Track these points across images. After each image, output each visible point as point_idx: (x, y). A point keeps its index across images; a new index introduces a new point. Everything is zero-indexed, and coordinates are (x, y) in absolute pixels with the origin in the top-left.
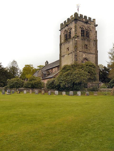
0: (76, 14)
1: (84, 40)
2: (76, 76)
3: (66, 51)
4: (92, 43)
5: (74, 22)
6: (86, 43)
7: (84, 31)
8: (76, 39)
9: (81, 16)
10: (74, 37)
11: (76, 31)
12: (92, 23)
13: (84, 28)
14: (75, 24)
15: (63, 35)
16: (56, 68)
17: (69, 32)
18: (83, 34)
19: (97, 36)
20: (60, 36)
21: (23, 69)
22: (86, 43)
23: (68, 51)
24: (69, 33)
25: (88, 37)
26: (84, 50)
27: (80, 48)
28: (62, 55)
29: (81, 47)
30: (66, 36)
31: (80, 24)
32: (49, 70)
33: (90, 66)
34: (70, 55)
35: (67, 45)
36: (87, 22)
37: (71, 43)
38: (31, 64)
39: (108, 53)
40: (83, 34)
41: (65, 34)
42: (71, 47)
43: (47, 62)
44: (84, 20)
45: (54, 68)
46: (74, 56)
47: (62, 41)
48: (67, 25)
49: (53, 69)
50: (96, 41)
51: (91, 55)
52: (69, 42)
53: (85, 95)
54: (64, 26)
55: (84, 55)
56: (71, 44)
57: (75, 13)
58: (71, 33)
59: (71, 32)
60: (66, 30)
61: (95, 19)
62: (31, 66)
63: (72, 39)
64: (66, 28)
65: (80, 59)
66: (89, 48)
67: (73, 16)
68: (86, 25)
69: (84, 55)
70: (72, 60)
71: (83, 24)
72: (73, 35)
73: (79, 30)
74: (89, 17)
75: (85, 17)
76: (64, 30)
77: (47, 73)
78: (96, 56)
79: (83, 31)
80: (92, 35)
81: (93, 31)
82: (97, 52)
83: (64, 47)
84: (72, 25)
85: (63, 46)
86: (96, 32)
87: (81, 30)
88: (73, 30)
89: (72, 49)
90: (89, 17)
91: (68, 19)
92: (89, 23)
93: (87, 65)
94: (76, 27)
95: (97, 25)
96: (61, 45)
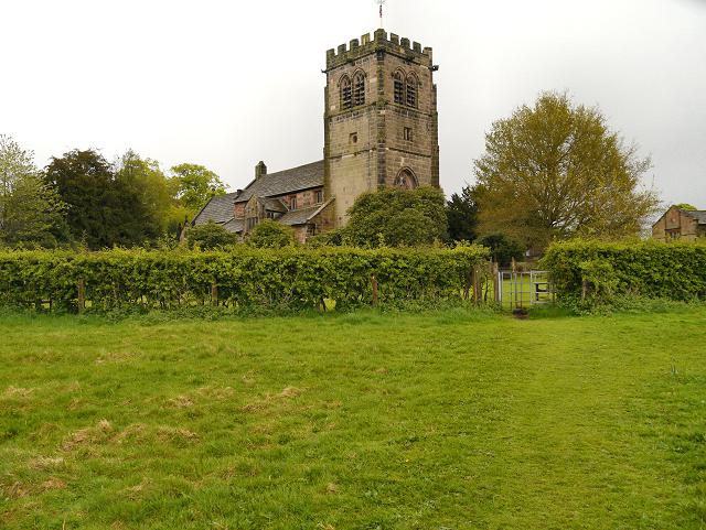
0: (380, 34)
1: (403, 112)
2: (406, 226)
3: (346, 140)
4: (423, 124)
5: (374, 58)
6: (408, 122)
7: (400, 84)
8: (383, 112)
9: (394, 38)
10: (374, 104)
11: (381, 84)
12: (423, 60)
13: (403, 78)
14: (379, 64)
15: (337, 89)
16: (308, 192)
17: (356, 82)
18: (400, 93)
19: (435, 100)
20: (326, 89)
21: (57, 164)
22: (408, 122)
23: (353, 144)
24: (358, 86)
25: (413, 103)
26: (403, 144)
27: (391, 139)
28: (334, 151)
29: (394, 136)
30: (346, 94)
31: (392, 63)
32: (280, 199)
33: (431, 198)
34: (363, 158)
35: (349, 125)
36: (409, 60)
37: (365, 120)
38: (153, 159)
39: (471, 162)
40: (400, 93)
41: (343, 87)
42: (366, 132)
43: (262, 168)
44: (402, 51)
45: (302, 194)
46: (374, 161)
47: (333, 108)
48: (351, 62)
49: (299, 196)
50: (433, 116)
51: (421, 161)
52: (358, 115)
53: (325, 313)
54: (340, 60)
55: (403, 159)
56: (363, 124)
57: (379, 30)
58: (363, 89)
59: (363, 84)
60: (346, 76)
61: (430, 49)
62: (149, 167)
63: (369, 110)
64: (348, 69)
65: (392, 172)
66: (414, 138)
67: (372, 38)
68: (407, 68)
69: (403, 159)
70: (369, 174)
71: (399, 63)
72: (371, 95)
73: (390, 83)
74: (414, 43)
75: (405, 42)
76: (339, 73)
77: (277, 209)
78: (433, 163)
79: (398, 86)
80: (423, 95)
81: (426, 85)
82: (435, 150)
83: (338, 128)
84: (370, 66)
85: (335, 125)
86: (434, 88)
87: (396, 83)
88: (373, 81)
89: (367, 137)
90: (414, 43)
91: (354, 42)
92: (416, 60)
93: (424, 197)
94: (380, 74)
95: (436, 68)
96: (328, 119)
